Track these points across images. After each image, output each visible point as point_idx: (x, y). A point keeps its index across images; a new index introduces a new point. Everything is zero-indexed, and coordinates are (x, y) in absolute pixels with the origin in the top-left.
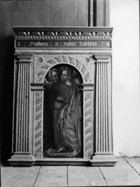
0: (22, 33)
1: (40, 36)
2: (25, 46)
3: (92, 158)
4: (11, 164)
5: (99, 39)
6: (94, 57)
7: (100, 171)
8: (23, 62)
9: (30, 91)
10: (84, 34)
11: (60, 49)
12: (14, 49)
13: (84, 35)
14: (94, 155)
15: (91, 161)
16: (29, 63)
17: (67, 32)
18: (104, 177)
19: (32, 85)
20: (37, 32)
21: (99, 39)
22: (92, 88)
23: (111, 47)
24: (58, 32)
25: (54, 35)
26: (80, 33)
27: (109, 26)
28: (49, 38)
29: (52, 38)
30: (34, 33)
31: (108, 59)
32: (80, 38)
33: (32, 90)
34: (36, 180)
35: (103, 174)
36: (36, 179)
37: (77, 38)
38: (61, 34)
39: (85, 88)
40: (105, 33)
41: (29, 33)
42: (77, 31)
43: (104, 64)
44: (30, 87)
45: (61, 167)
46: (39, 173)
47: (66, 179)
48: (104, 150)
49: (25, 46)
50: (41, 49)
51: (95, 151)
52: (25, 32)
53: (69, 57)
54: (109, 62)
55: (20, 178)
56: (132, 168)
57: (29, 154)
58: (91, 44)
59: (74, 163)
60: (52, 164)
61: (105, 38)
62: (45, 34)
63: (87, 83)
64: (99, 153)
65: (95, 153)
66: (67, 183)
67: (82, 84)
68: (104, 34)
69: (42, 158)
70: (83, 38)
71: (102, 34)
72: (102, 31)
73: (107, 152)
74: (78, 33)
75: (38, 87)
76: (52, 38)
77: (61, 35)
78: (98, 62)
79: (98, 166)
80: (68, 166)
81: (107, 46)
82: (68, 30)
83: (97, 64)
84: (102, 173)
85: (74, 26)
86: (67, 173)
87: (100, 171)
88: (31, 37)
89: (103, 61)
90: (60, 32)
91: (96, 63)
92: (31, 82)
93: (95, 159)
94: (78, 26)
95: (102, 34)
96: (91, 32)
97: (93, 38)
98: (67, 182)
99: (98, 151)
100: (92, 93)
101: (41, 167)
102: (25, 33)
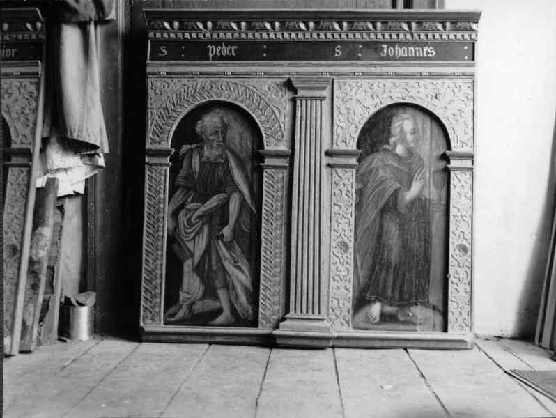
0: (159, 25)
4: (279, 342)
6: (289, 85)
8: (306, 98)
9: (324, 168)
10: (286, 26)
11: (352, 64)
12: (145, 65)
14: (284, 319)
15: (276, 332)
16: (322, 99)
18: (422, 375)
19: (327, 154)
20: (331, 22)
21: (233, 38)
22: (285, 162)
23: (473, 59)
27: (443, 7)
28: (188, 34)
29: (301, 36)
30: (257, 24)
31: (325, 88)
32: (344, 36)
33: (329, 165)
34: (265, 375)
36: (265, 372)
37: (372, 36)
38: (288, 26)
39: (268, 162)
40: (443, 23)
43: (309, 102)
44: (325, 160)
45: (194, 345)
47: (334, 374)
48: (310, 311)
51: (287, 310)
52: (30, 23)
53: (226, 82)
55: (228, 369)
56: (488, 359)
57: (323, 320)
58: (220, 52)
59: (452, 343)
61: (441, 36)
62: (283, 27)
63: (154, 147)
64: (298, 315)
65: (286, 316)
66: (336, 381)
68: (439, 26)
69: (162, 325)
70: (351, 36)
71: (434, 28)
72: (365, 19)
73: (316, 316)
75: (160, 159)
76: (265, 35)
78: (298, 97)
79: (333, 347)
80: (336, 349)
82: (352, 18)
83: (298, 103)
84: (417, 367)
85: (356, 8)
86: (336, 363)
87: (413, 361)
88: (351, 36)
89: (311, 95)
91: (294, 100)
92: (326, 147)
93: (287, 329)
94: (366, 7)
95: (434, 28)
96: (304, 22)
97: (261, 37)
98: (338, 380)
100: (286, 172)
101: (209, 348)
102: (166, 25)
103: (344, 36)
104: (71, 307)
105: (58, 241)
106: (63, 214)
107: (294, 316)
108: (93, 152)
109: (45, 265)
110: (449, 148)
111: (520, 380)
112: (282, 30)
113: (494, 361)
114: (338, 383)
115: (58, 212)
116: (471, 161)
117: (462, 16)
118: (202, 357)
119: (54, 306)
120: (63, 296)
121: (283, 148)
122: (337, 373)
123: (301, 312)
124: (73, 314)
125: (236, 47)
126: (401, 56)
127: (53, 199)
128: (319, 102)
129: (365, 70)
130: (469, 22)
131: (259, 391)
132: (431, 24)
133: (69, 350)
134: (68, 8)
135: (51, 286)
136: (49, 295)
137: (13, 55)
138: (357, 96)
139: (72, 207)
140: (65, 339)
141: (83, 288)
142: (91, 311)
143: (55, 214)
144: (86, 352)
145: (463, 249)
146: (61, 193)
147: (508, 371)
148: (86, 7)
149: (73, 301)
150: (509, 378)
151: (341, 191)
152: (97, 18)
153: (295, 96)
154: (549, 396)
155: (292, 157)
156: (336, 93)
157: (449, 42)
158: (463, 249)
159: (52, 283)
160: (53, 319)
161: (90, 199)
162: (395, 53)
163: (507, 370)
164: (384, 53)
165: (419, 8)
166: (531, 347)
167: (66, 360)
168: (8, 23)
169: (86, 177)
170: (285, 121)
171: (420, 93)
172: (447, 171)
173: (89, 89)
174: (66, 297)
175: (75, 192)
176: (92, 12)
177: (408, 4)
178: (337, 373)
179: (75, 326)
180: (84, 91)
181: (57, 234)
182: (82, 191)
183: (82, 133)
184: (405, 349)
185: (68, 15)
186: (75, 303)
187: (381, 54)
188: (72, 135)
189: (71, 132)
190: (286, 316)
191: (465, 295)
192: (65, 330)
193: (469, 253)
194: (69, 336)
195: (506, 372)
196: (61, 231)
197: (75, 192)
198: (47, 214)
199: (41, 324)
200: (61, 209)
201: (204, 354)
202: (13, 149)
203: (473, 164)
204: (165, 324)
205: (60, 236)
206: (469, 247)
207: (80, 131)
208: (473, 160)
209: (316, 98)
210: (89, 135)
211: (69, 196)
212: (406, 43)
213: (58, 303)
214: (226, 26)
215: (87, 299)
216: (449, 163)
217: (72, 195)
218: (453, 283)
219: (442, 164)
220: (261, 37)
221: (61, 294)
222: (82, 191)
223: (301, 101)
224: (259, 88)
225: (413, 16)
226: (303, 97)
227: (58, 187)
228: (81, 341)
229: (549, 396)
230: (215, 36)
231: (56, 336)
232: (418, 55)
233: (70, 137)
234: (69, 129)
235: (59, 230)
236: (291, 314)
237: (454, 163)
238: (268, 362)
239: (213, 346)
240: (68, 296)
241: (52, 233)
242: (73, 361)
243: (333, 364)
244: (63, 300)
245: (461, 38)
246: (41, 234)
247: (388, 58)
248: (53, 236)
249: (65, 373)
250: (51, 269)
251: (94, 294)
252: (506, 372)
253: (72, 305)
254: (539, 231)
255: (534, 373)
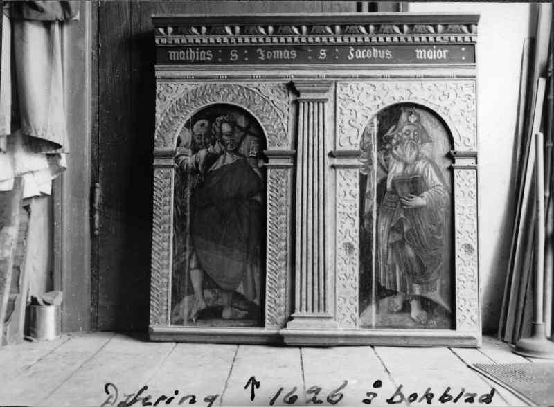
1: (198, 36)
2: (220, 60)
3: (285, 326)
5: (230, 42)
6: (291, 87)
7: (379, 357)
8: (309, 101)
11: (398, 67)
13: (314, 33)
14: (291, 319)
15: (283, 331)
16: (324, 101)
17: (431, 25)
19: (331, 155)
20: (291, 26)
22: (289, 162)
23: (475, 62)
24: (409, 26)
25: (264, 33)
26: (440, 28)
27: (407, 10)
28: (218, 41)
32: (268, 40)
34: (231, 372)
35: (385, 362)
36: (231, 368)
39: (272, 162)
40: (435, 27)
41: (271, 29)
42: (432, 23)
46: (237, 357)
49: (220, 60)
50: (192, 69)
51: (293, 310)
54: (327, 100)
57: (329, 318)
60: (191, 338)
62: (210, 32)
63: (276, 148)
64: (304, 313)
65: (293, 315)
67: (264, 151)
70: (275, 40)
73: (322, 314)
74: (435, 27)
77: (347, 33)
78: (301, 100)
81: (321, 57)
83: (301, 105)
84: (382, 362)
90: (345, 26)
91: (296, 103)
92: (329, 148)
93: (293, 328)
97: (435, 40)
98: (303, 376)
99: (319, 311)
100: (289, 172)
102: (161, 30)
103: (268, 40)
104: (37, 307)
105: (24, 241)
106: (29, 214)
107: (305, 315)
108: (53, 152)
109: (11, 264)
110: (453, 148)
111: (482, 374)
112: (377, 33)
113: (458, 356)
114: (303, 378)
115: (24, 211)
116: (475, 160)
117: (453, 19)
118: (169, 355)
119: (20, 305)
120: (30, 295)
121: (287, 147)
122: (303, 369)
123: (307, 310)
124: (39, 315)
125: (447, 51)
126: (199, 60)
127: (19, 200)
128: (321, 104)
129: (230, 73)
130: (460, 24)
131: (223, 388)
132: (390, 27)
133: (36, 349)
134: (35, 7)
135: (17, 284)
136: (15, 295)
137: (445, 57)
138: (356, 100)
139: (39, 209)
140: (30, 338)
141: (50, 287)
142: (58, 310)
143: (21, 213)
144: (52, 352)
145: (468, 248)
146: (27, 194)
147: (471, 365)
148: (53, 9)
149: (39, 300)
150: (472, 372)
151: (463, 193)
152: (63, 17)
153: (298, 98)
154: (509, 389)
155: (295, 157)
156: (338, 95)
157: (309, 45)
158: (468, 248)
159: (18, 282)
160: (18, 320)
161: (57, 198)
162: (372, 55)
163: (469, 365)
164: (351, 56)
165: (384, 11)
166: (494, 341)
167: (32, 360)
168: (171, 26)
169: (52, 178)
170: (288, 122)
171: (420, 93)
172: (451, 169)
173: (53, 89)
174: (32, 297)
175: (41, 193)
176: (58, 13)
177: (373, 8)
178: (303, 369)
179: (42, 326)
180: (49, 92)
181: (23, 233)
182: (49, 192)
183: (46, 132)
184: (372, 347)
185: (34, 14)
186: (41, 303)
187: (349, 57)
188: (36, 133)
189: (35, 130)
190: (293, 315)
191: (472, 292)
192: (31, 329)
193: (476, 253)
194: (36, 336)
195: (469, 367)
196: (26, 231)
197: (41, 193)
198: (13, 214)
199: (7, 323)
200: (27, 208)
201: (171, 352)
202: (269, 152)
203: (476, 163)
204: (171, 323)
205: (26, 236)
206: (475, 247)
207: (45, 130)
208: (476, 159)
209: (318, 101)
210: (53, 134)
211: (36, 197)
212: (364, 46)
213: (25, 303)
214: (389, 30)
215: (54, 297)
216: (454, 163)
217: (38, 196)
218: (459, 280)
219: (448, 163)
220: (435, 40)
221: (28, 294)
222: (49, 192)
223: (304, 103)
224: (260, 90)
225: (337, 20)
226: (305, 100)
227: (24, 187)
228: (47, 340)
229: (509, 389)
230: (177, 41)
231: (22, 336)
232: (275, 57)
233: (34, 135)
234: (33, 128)
235: (24, 230)
236: (297, 313)
237: (459, 162)
238: (234, 359)
239: (179, 344)
240: (35, 296)
241: (17, 233)
242: (39, 360)
243: (299, 359)
244: (29, 300)
245: (354, 40)
246: (7, 234)
247: (355, 61)
248: (19, 235)
249: (31, 372)
250: (17, 269)
251: (61, 293)
252: (469, 367)
253: (39, 305)
254: (501, 228)
255: (495, 367)
